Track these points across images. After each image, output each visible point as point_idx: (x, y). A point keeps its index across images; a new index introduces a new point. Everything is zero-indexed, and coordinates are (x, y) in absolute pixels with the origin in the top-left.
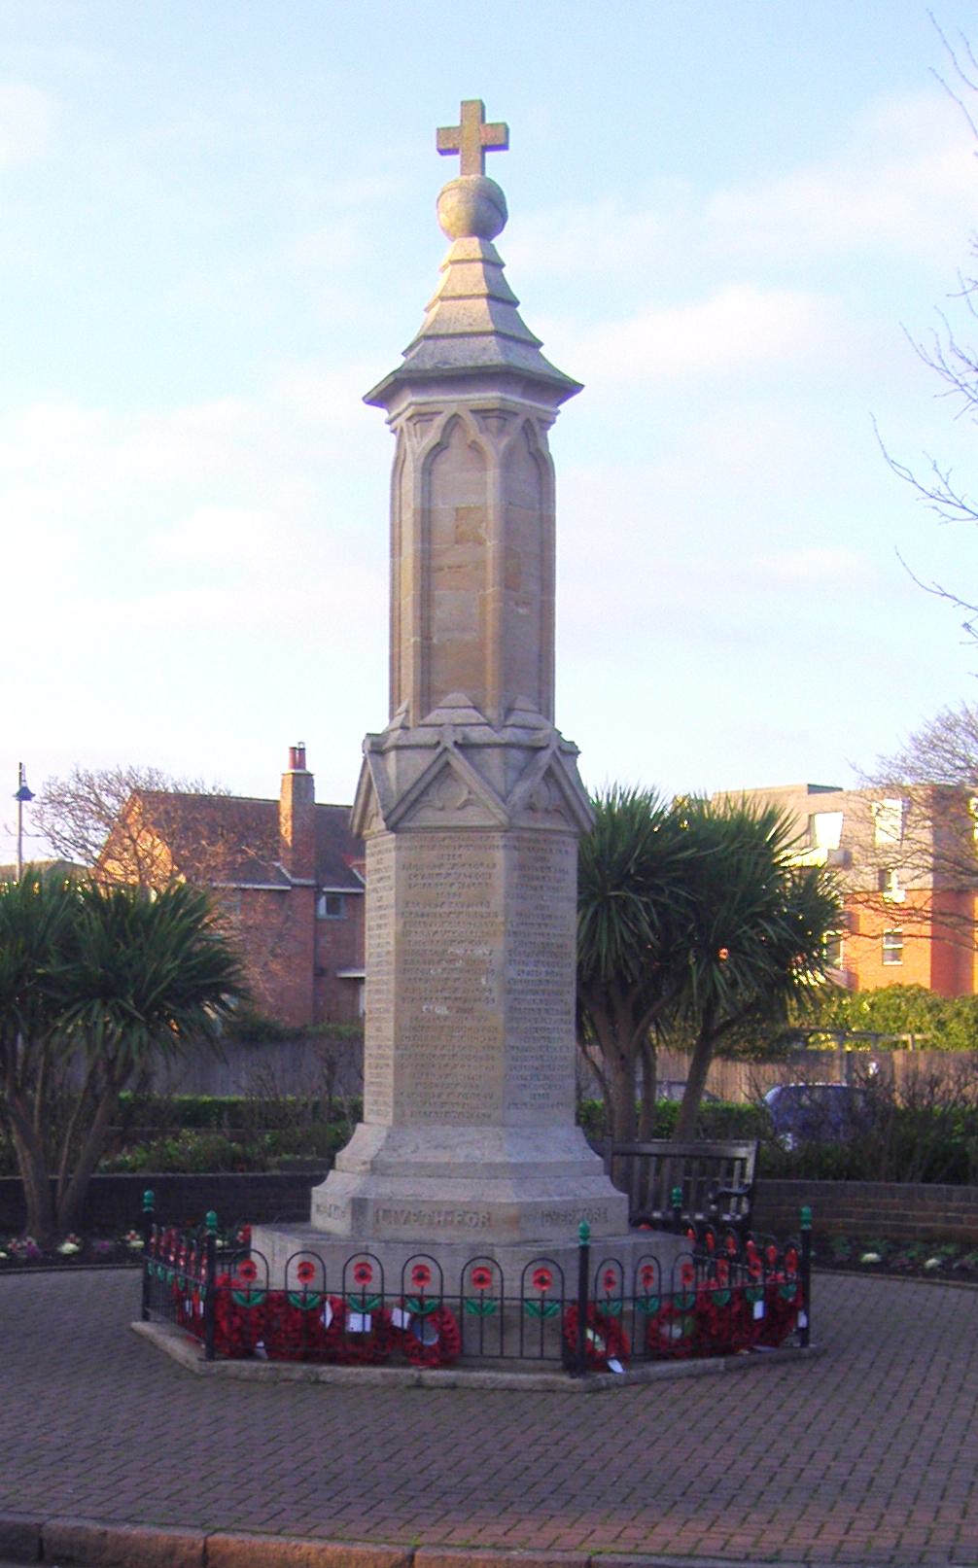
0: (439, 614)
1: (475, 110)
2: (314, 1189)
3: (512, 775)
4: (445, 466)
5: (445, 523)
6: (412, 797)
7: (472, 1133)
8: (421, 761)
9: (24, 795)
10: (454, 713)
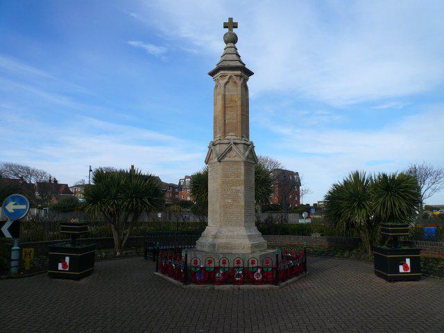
0: (227, 117)
1: (231, 19)
8: (225, 147)
9: (91, 170)
10: (231, 137)
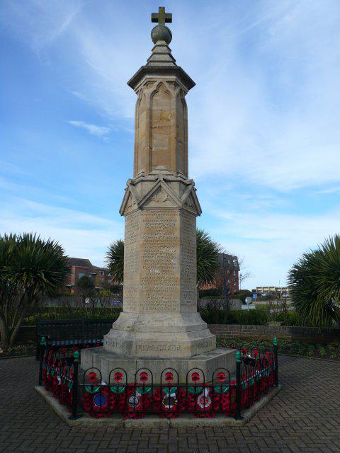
0: (154, 141)
2: (246, 284)
3: (181, 192)
4: (156, 98)
5: (156, 114)
6: (148, 197)
7: (169, 315)
8: (149, 186)
